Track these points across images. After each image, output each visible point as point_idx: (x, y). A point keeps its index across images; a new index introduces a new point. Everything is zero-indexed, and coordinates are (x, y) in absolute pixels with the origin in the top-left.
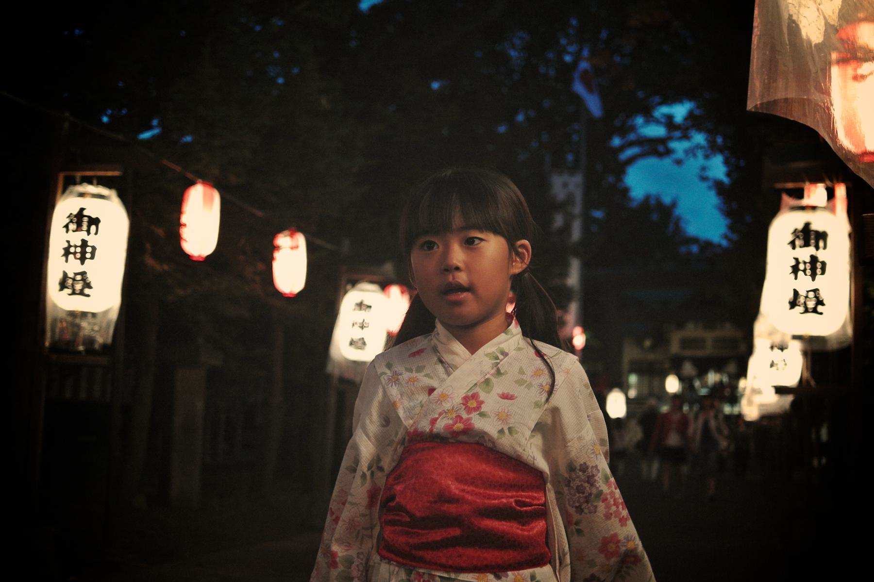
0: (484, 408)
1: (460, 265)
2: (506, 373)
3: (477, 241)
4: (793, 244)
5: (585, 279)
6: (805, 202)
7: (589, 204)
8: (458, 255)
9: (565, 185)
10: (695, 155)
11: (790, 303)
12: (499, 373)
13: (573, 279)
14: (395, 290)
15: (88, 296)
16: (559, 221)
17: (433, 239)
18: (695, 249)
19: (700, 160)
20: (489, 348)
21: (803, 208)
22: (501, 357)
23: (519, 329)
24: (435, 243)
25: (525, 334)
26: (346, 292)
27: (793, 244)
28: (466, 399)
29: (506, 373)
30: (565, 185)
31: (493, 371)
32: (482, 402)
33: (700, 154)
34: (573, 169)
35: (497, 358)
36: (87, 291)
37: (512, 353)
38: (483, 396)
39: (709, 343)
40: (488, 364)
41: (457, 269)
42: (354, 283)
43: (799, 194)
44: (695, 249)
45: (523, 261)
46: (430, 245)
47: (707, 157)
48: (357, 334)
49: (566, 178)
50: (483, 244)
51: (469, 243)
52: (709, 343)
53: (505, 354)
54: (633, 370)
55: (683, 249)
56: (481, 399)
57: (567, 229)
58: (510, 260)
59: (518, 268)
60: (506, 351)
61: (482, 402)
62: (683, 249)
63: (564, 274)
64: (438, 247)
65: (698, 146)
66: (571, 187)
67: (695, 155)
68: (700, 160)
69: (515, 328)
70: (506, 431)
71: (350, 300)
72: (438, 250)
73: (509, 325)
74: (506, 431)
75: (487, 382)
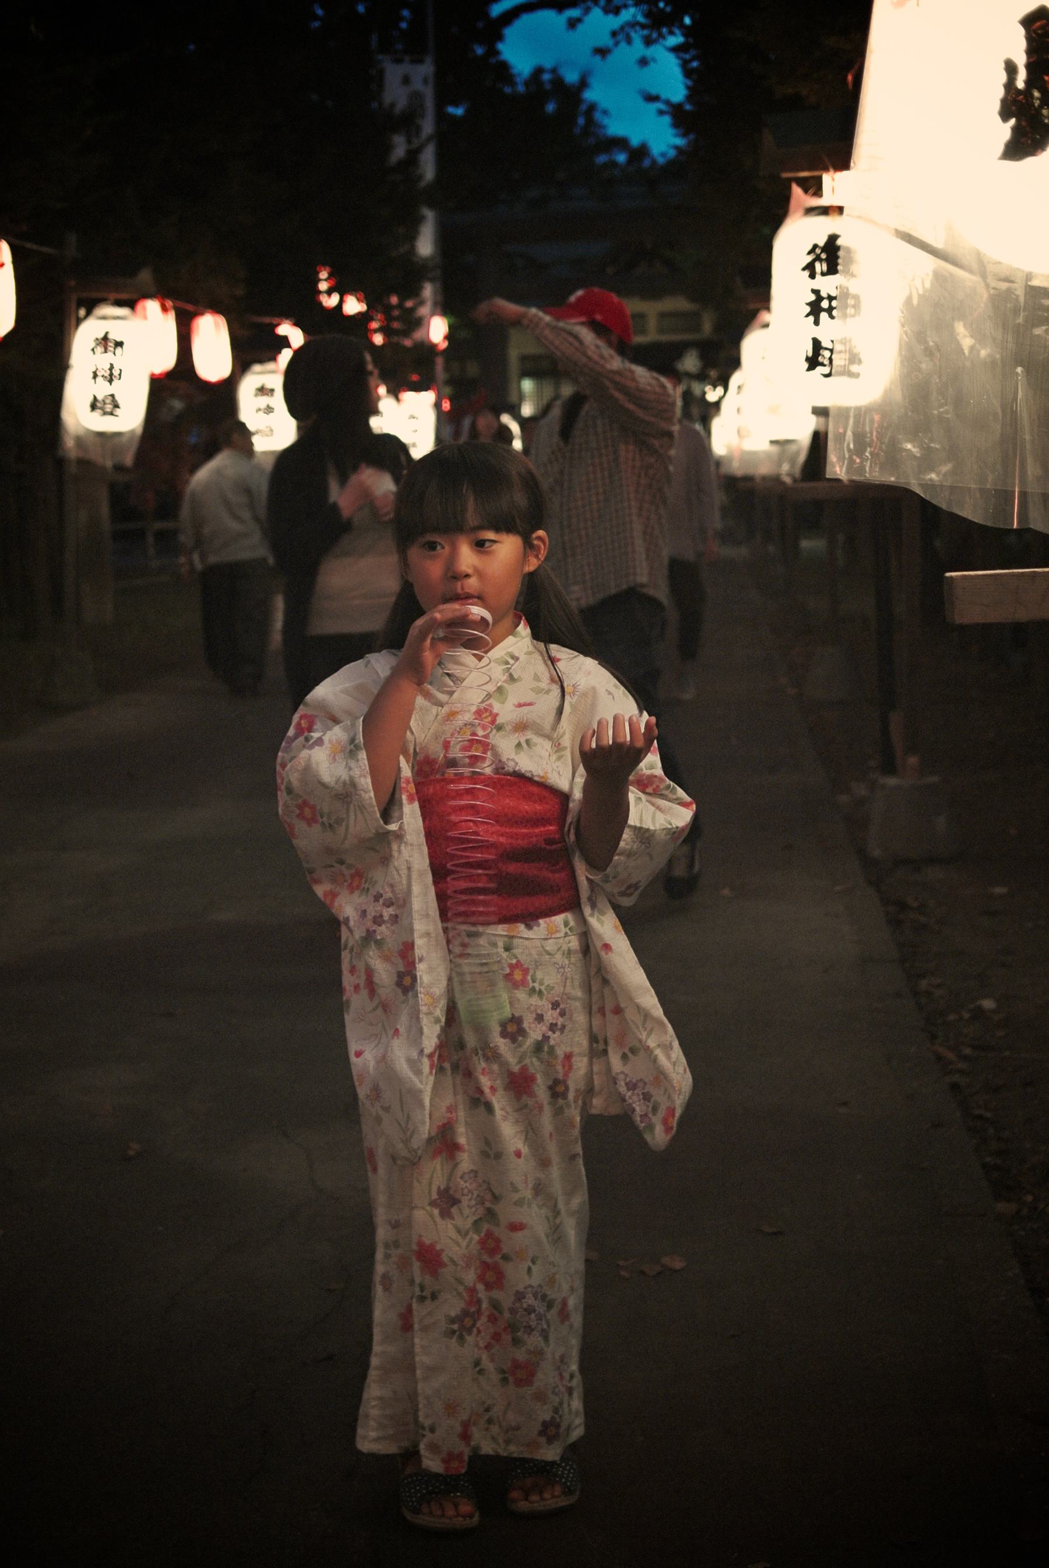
0: (499, 721)
1: (470, 571)
2: (519, 679)
3: (487, 544)
4: (810, 268)
5: (445, 239)
6: (824, 201)
7: (443, 99)
8: (467, 557)
9: (406, 80)
10: (629, 41)
11: (808, 359)
12: (512, 679)
13: (425, 246)
14: (152, 306)
15: (857, 376)
16: (399, 150)
17: (438, 540)
18: (621, 158)
19: (638, 48)
20: (498, 652)
21: (825, 211)
22: (511, 661)
23: (528, 630)
24: (435, 543)
25: (536, 636)
26: (79, 321)
27: (810, 268)
28: (479, 713)
29: (519, 679)
30: (406, 80)
31: (505, 678)
32: (497, 715)
33: (637, 37)
34: (415, 51)
35: (507, 663)
36: (854, 368)
37: (523, 657)
38: (497, 707)
39: (652, 323)
40: (498, 673)
41: (467, 576)
42: (90, 306)
43: (814, 187)
44: (621, 158)
45: (537, 556)
46: (432, 546)
47: (648, 42)
48: (102, 389)
49: (405, 68)
50: (495, 547)
51: (480, 545)
52: (652, 323)
53: (516, 659)
54: (526, 374)
55: (602, 159)
56: (495, 711)
57: (412, 157)
58: (525, 557)
59: (532, 565)
60: (517, 654)
61: (497, 715)
62: (602, 159)
63: (412, 237)
64: (443, 548)
65: (633, 24)
66: (418, 85)
67: (629, 41)
68: (638, 48)
69: (524, 629)
70: (524, 745)
71: (85, 336)
72: (444, 551)
73: (518, 625)
74: (524, 745)
75: (500, 690)
